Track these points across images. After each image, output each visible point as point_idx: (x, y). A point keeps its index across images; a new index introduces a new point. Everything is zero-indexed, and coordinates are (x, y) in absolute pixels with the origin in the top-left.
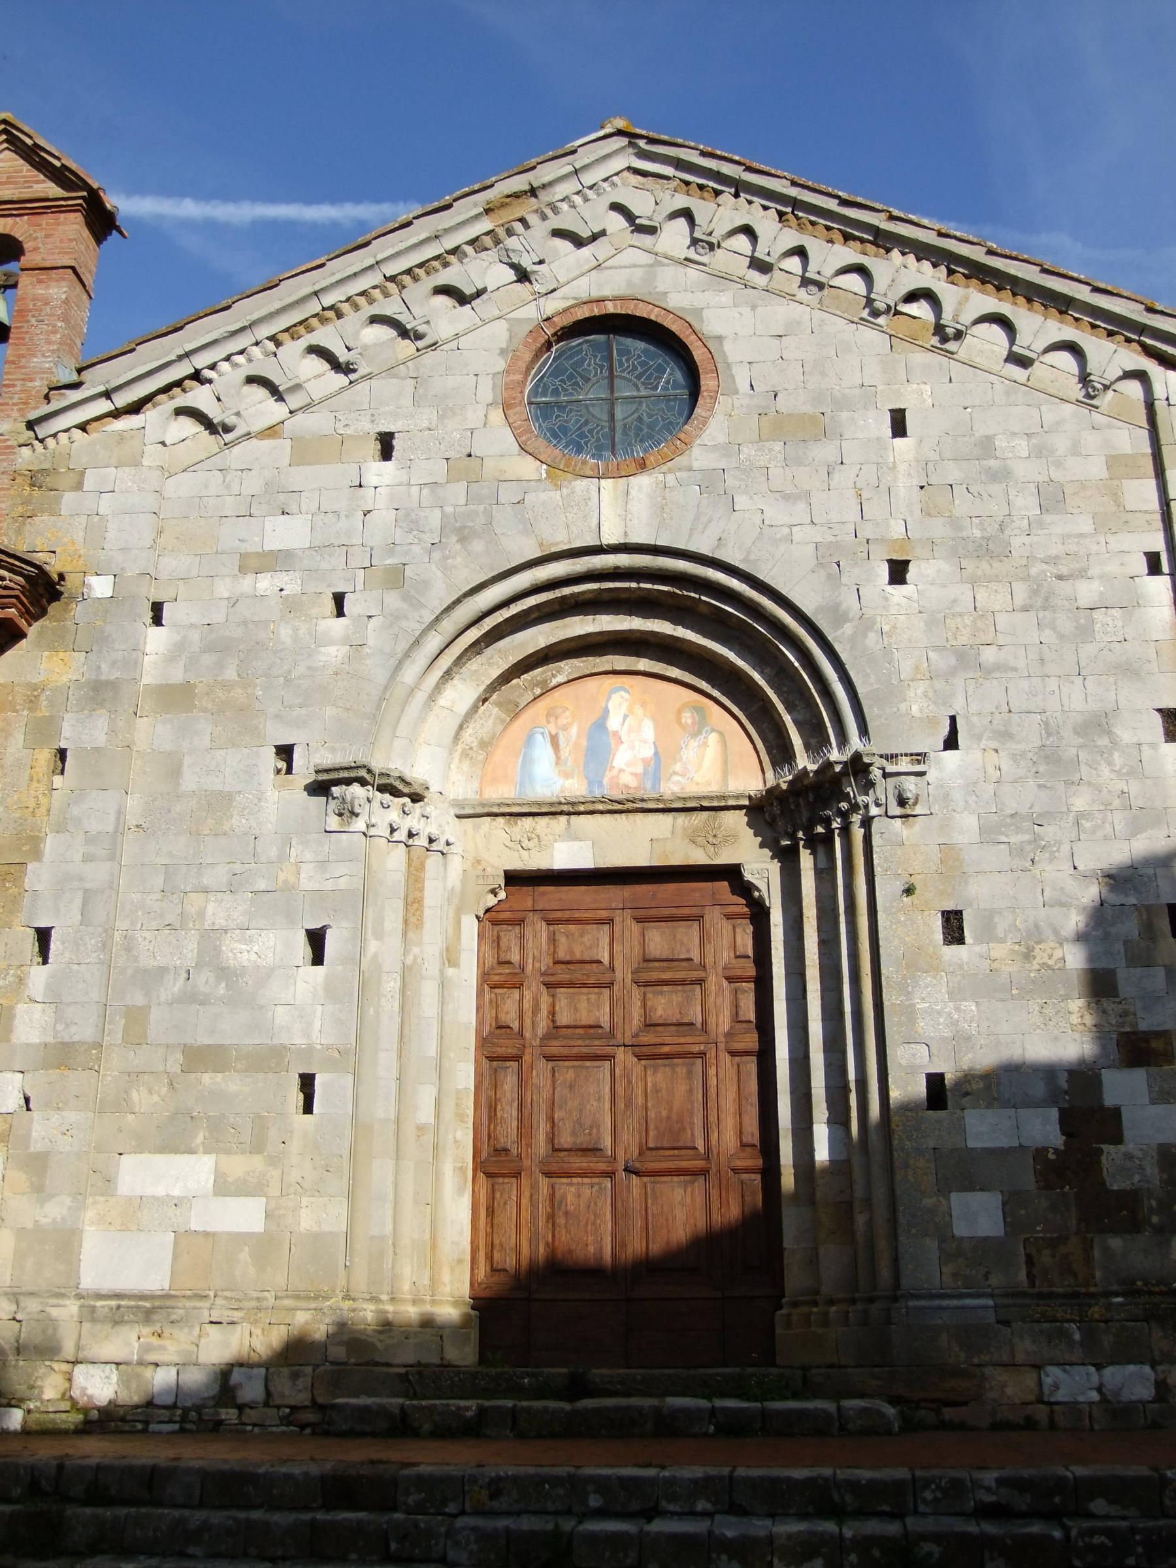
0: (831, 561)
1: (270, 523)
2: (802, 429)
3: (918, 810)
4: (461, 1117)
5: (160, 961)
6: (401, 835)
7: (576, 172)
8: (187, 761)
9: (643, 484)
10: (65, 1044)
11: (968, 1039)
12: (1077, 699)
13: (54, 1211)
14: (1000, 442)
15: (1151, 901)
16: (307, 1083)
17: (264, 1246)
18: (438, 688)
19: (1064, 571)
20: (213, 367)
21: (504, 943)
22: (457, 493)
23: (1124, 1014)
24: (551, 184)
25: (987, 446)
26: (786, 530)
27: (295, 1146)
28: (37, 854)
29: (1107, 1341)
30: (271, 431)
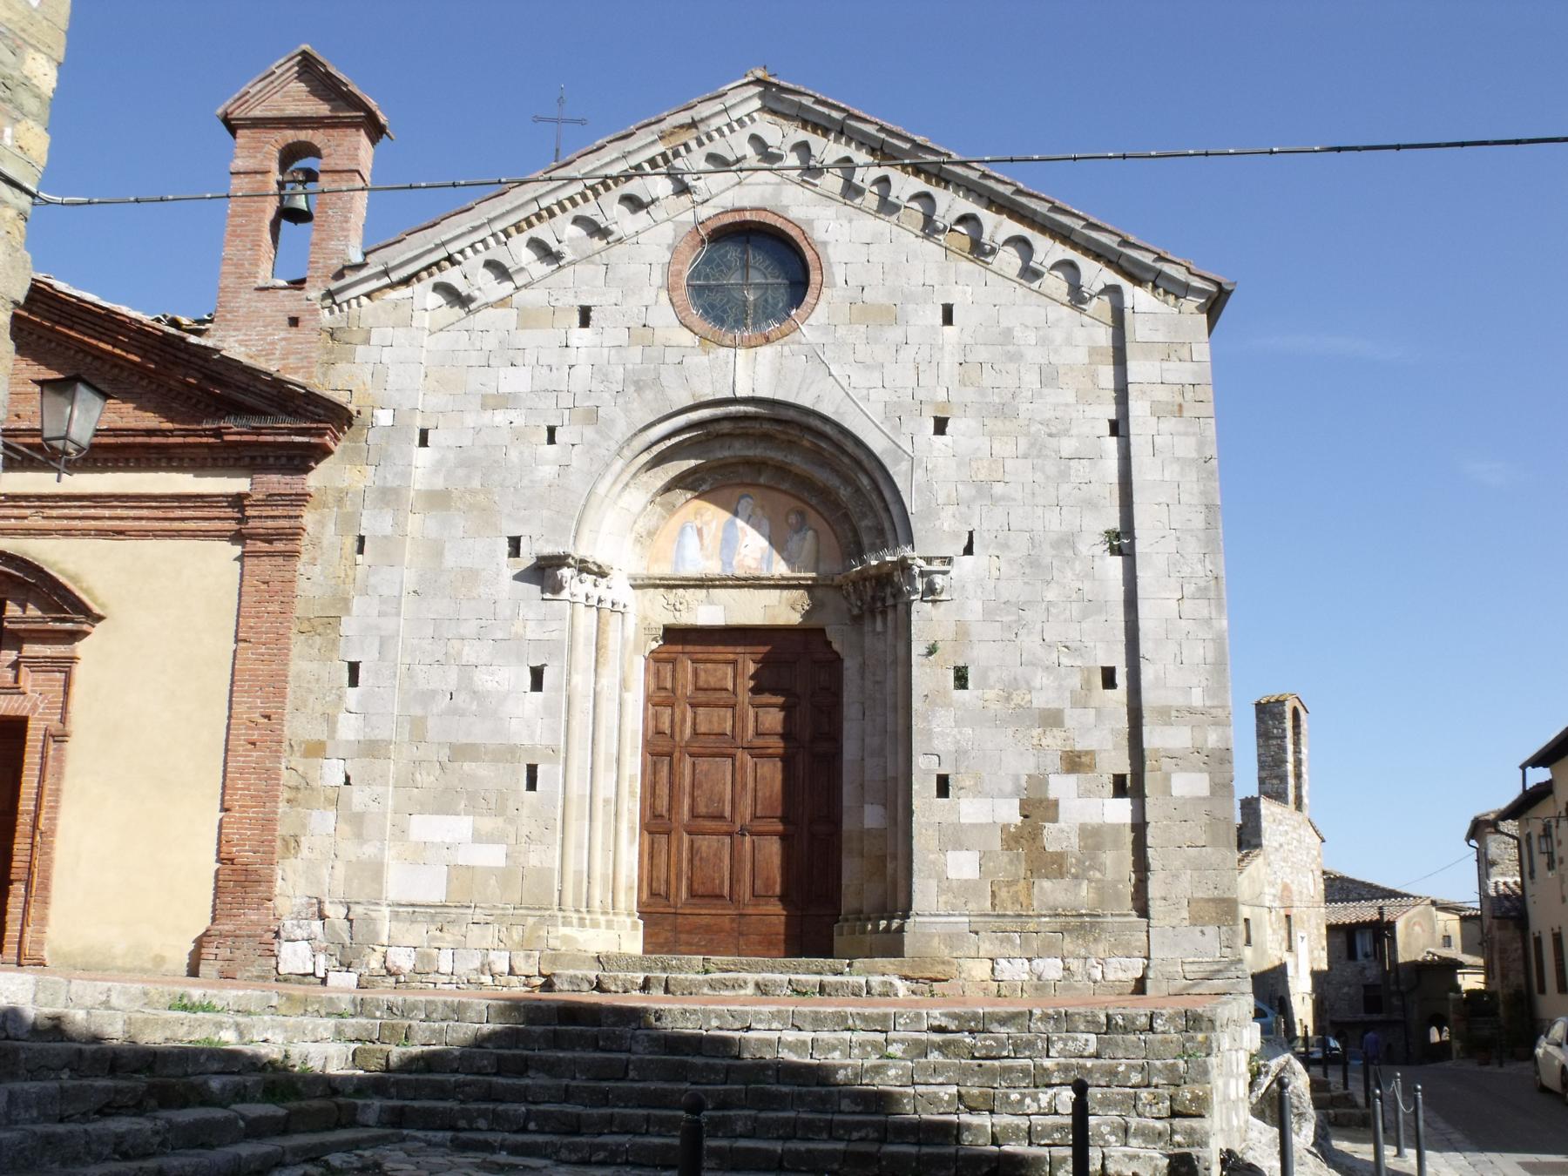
0: (894, 414)
1: (502, 372)
2: (880, 316)
3: (943, 597)
4: (632, 793)
6: (594, 601)
7: (726, 110)
8: (448, 545)
9: (767, 351)
10: (371, 742)
11: (966, 752)
12: (1055, 523)
13: (369, 850)
14: (1017, 333)
15: (1091, 664)
16: (532, 771)
17: (503, 876)
18: (619, 495)
19: (1054, 431)
20: (461, 252)
21: (662, 673)
22: (635, 353)
24: (708, 118)
25: (1008, 332)
26: (864, 392)
27: (525, 812)
28: (348, 610)
30: (503, 302)
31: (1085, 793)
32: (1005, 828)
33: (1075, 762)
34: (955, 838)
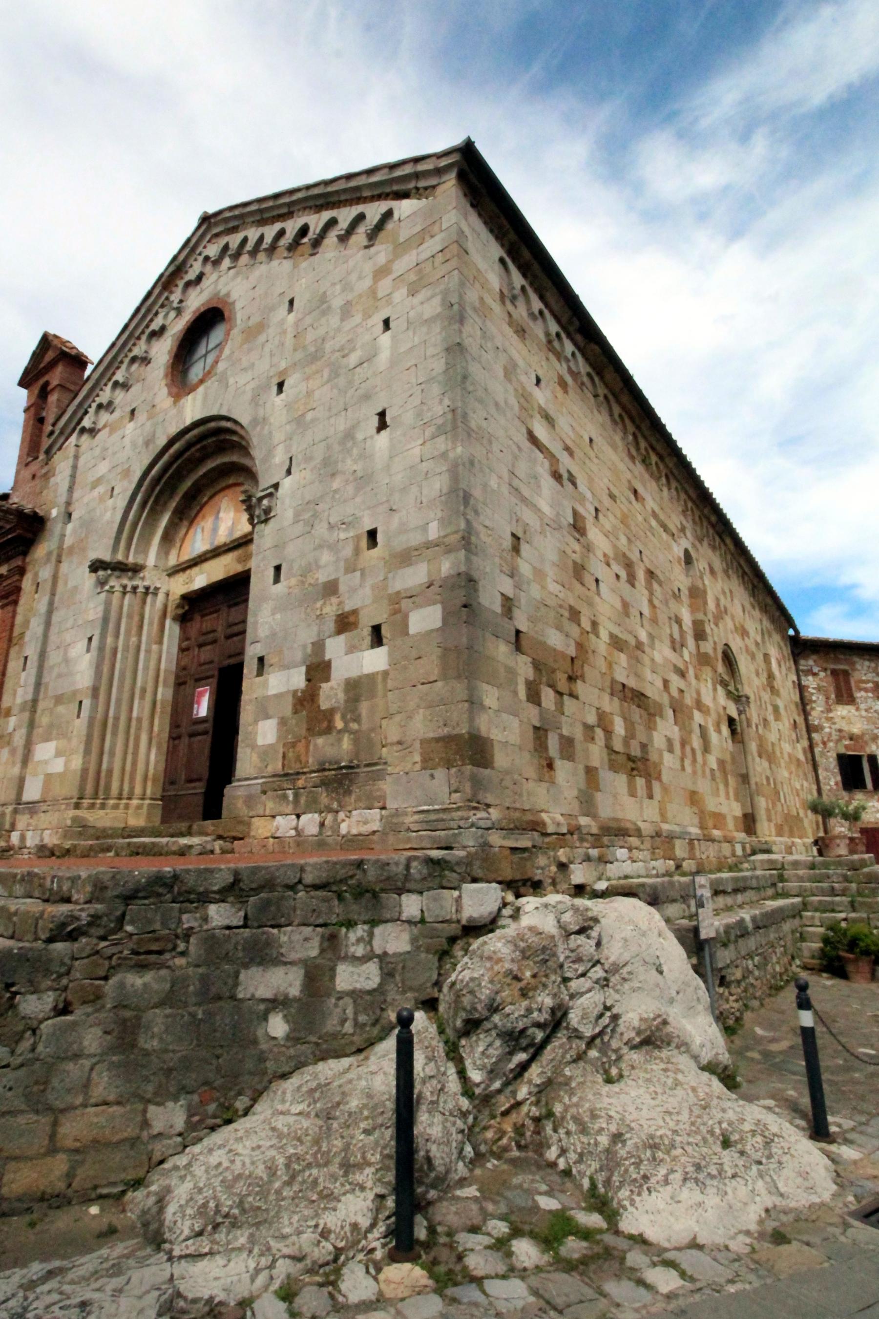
17: (467, 857)
29: (303, 800)
31: (351, 649)
33: (345, 623)
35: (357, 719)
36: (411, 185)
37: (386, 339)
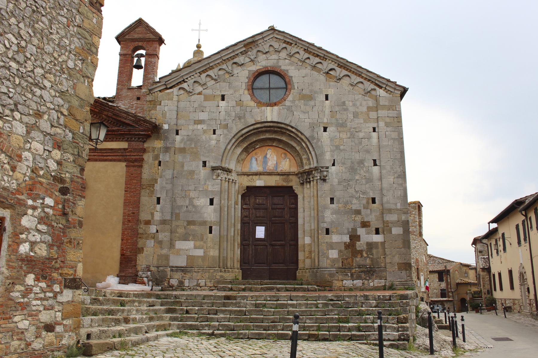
0: (312, 126)
4: (238, 234)
5: (181, 204)
12: (357, 157)
13: (164, 251)
17: (203, 258)
22: (238, 109)
23: (362, 218)
25: (344, 103)
27: (209, 240)
28: (157, 182)
29: (355, 276)
30: (200, 94)
31: (368, 233)
32: (345, 243)
33: (365, 225)
34: (331, 246)
35: (372, 254)
36: (384, 86)
37: (375, 135)
